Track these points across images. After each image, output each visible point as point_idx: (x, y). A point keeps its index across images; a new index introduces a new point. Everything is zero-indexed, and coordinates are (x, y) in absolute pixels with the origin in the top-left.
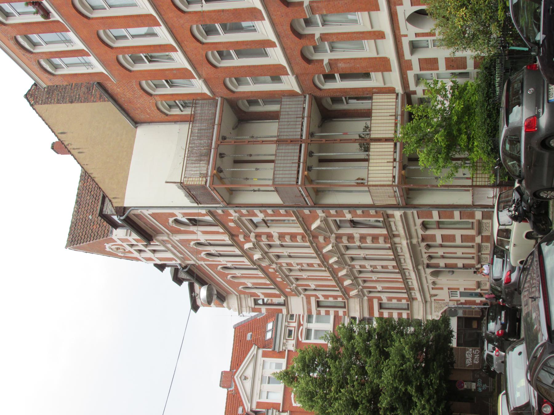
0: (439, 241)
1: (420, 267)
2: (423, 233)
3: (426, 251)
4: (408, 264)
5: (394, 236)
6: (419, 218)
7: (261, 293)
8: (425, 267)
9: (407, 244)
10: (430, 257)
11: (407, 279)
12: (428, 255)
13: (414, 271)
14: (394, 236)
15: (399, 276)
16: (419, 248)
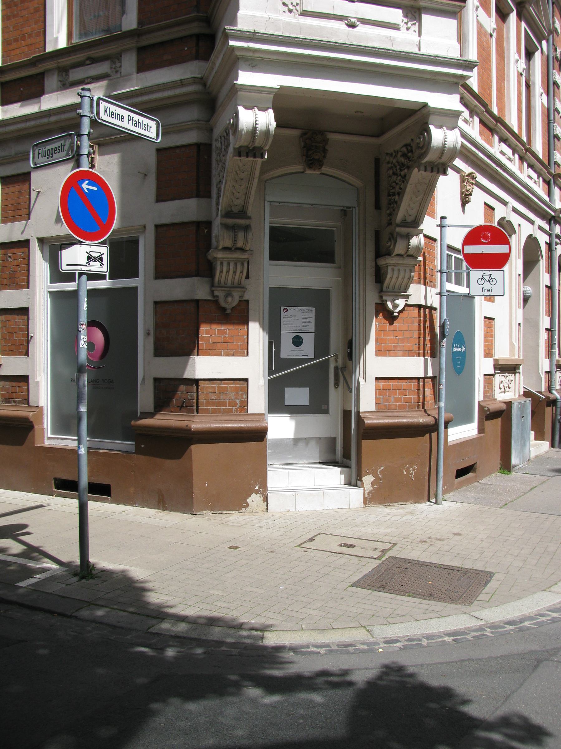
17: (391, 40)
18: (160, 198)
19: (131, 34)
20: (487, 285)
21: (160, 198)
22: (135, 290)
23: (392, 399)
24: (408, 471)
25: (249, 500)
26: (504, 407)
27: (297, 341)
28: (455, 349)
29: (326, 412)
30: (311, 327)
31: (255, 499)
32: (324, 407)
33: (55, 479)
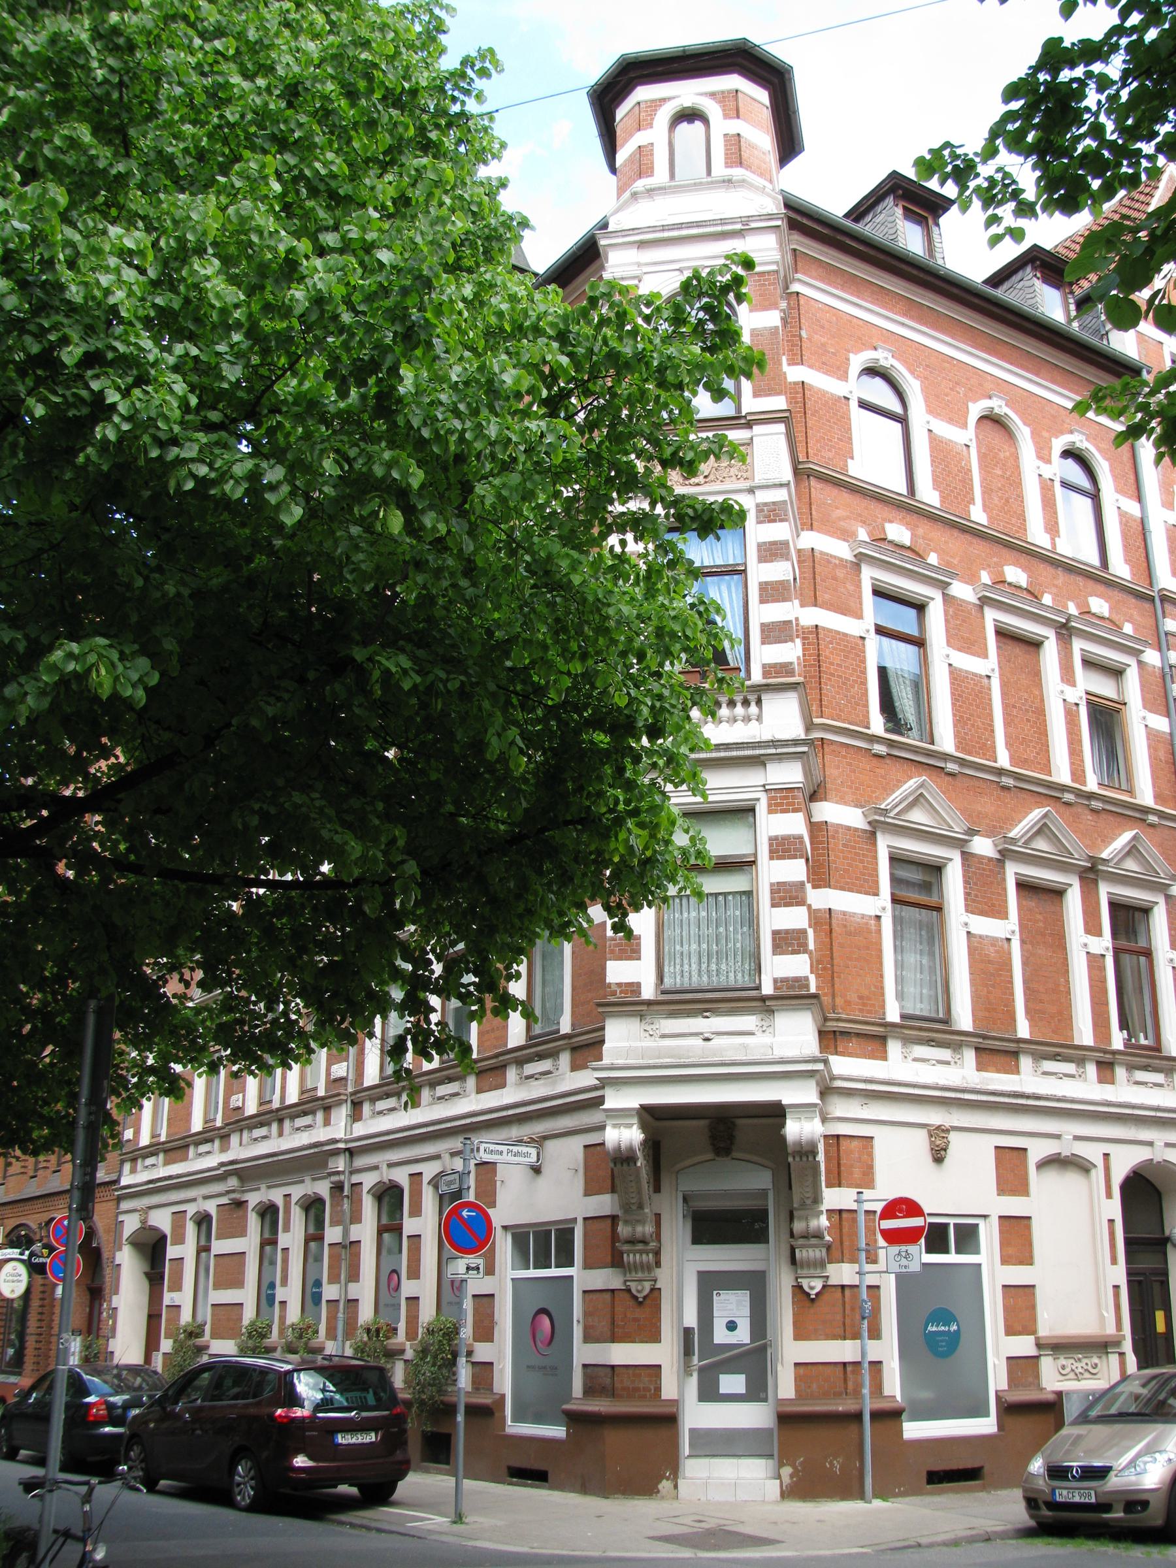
0: (220, 1246)
1: (233, 1182)
2: (366, 1188)
3: (294, 1199)
4: (242, 1149)
5: (357, 1105)
6: (586, 1147)
7: (712, 95)
8: (233, 1196)
9: (335, 1141)
10: (268, 1212)
11: (281, 1121)
12: (280, 1202)
13: (222, 1164)
14: (357, 1105)
15: (197, 1125)
16: (263, 1186)
17: (745, 1047)
18: (587, 1193)
19: (566, 1037)
20: (904, 1262)
21: (587, 1193)
22: (570, 1278)
23: (814, 1386)
24: (831, 1463)
25: (660, 1486)
26: (1051, 1397)
27: (731, 1326)
28: (932, 1328)
29: (765, 1400)
30: (746, 1311)
31: (665, 1485)
32: (762, 1395)
33: (509, 1468)
